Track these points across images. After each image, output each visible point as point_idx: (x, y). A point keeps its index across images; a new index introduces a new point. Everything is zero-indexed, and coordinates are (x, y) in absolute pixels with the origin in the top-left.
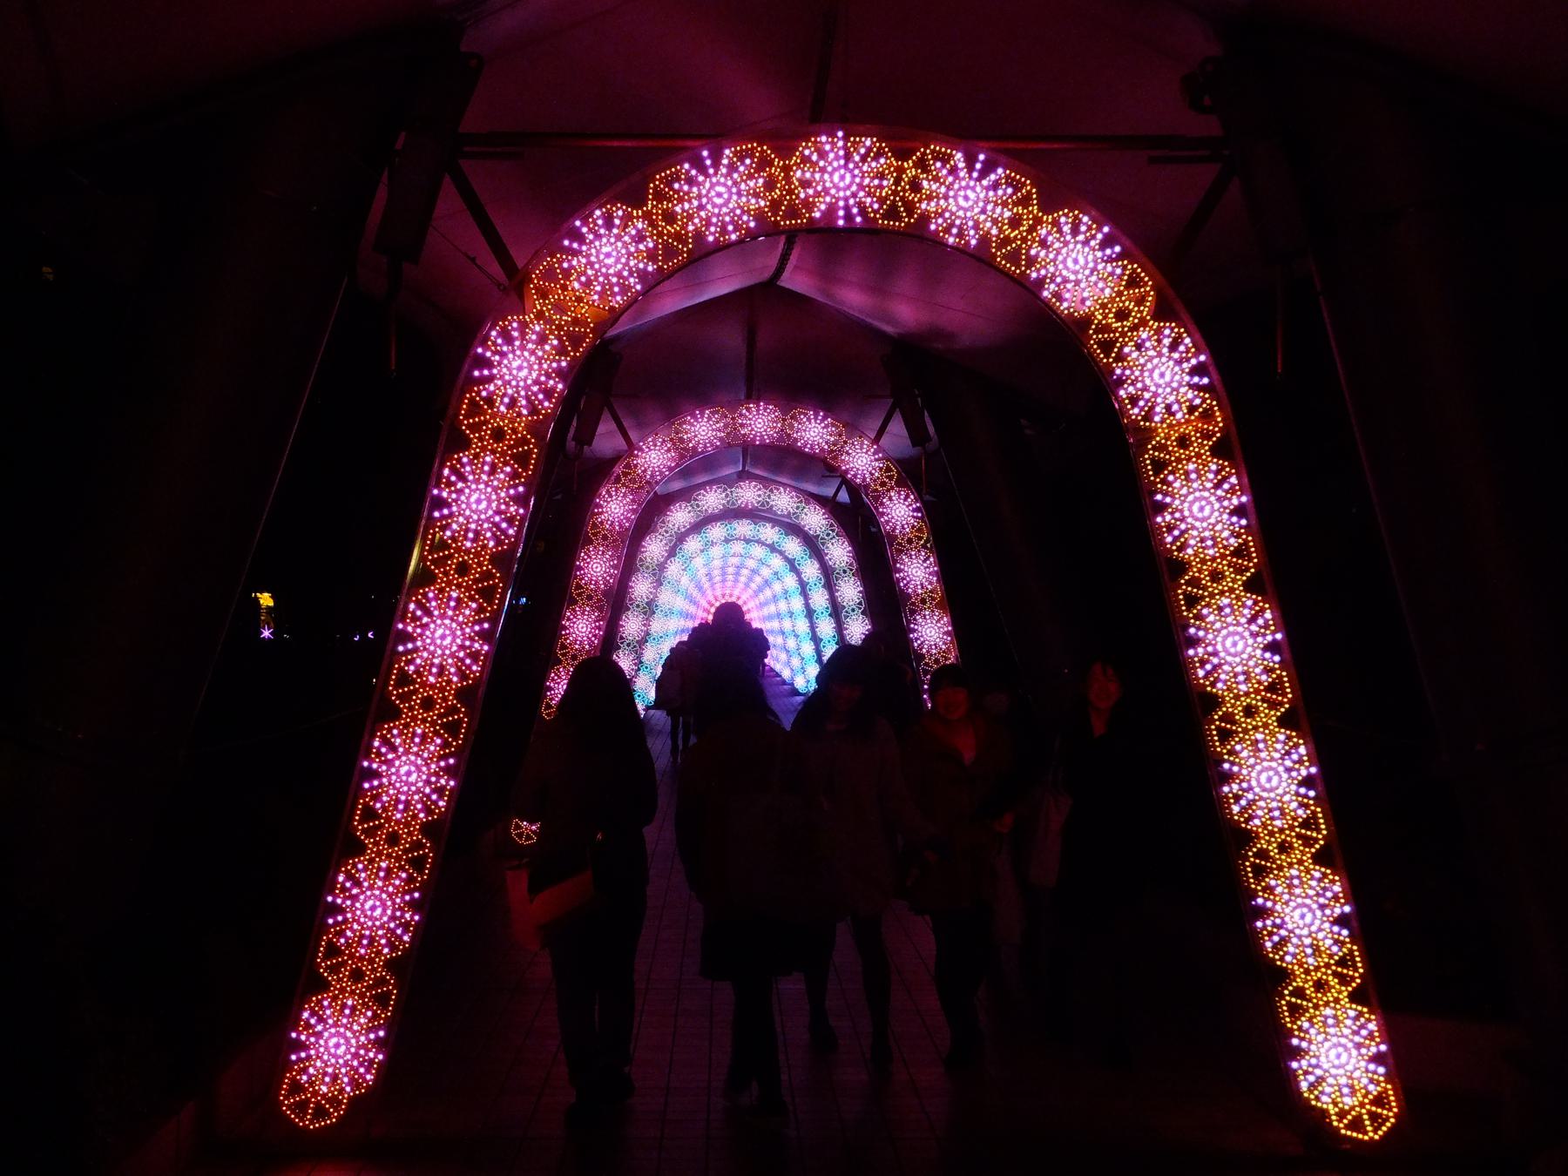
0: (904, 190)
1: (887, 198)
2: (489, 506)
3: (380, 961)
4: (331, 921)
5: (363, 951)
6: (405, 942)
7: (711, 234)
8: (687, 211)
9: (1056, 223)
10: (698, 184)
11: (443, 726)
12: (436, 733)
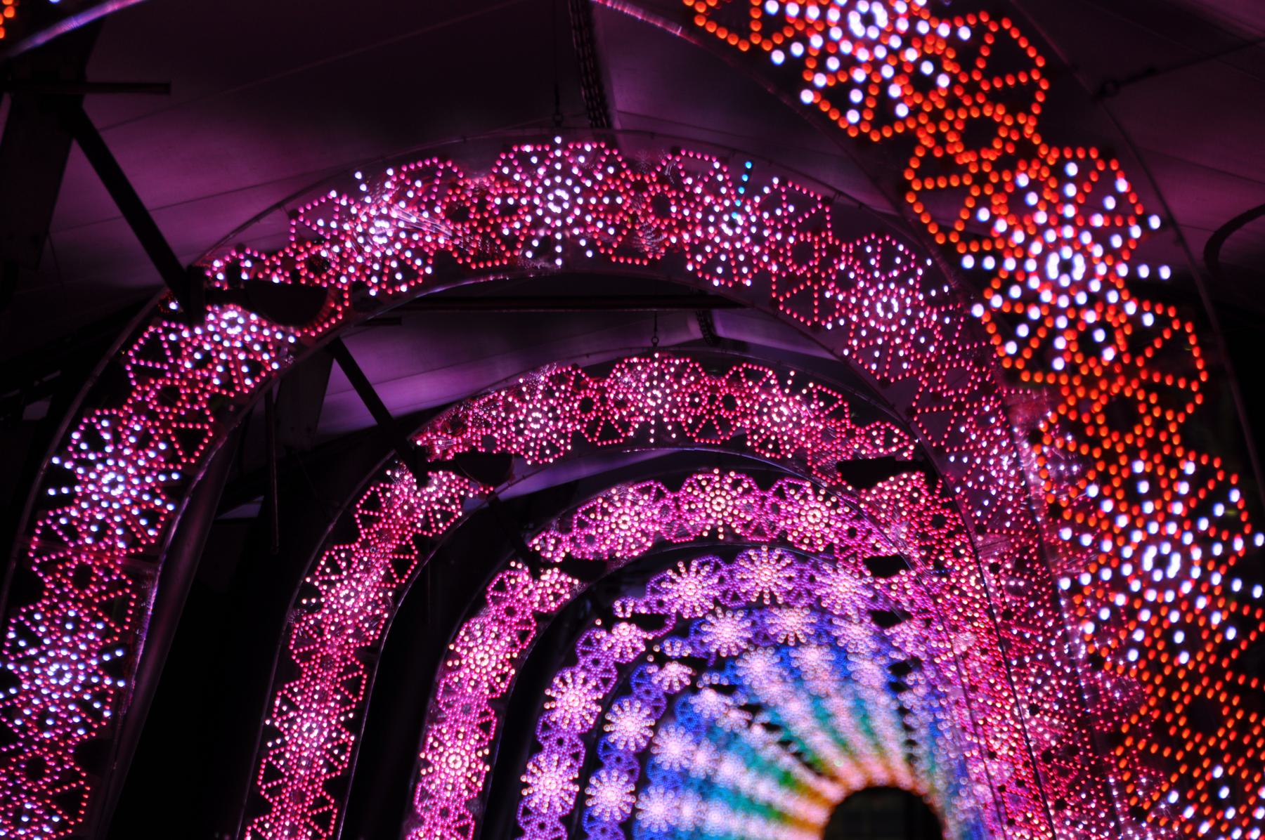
0: (718, 408)
1: (702, 416)
2: (320, 734)
3: (319, 783)
4: (270, 744)
5: (302, 772)
6: (344, 762)
7: (530, 458)
8: (505, 436)
9: (860, 255)
10: (515, 410)
11: (313, 818)
12: (307, 826)
